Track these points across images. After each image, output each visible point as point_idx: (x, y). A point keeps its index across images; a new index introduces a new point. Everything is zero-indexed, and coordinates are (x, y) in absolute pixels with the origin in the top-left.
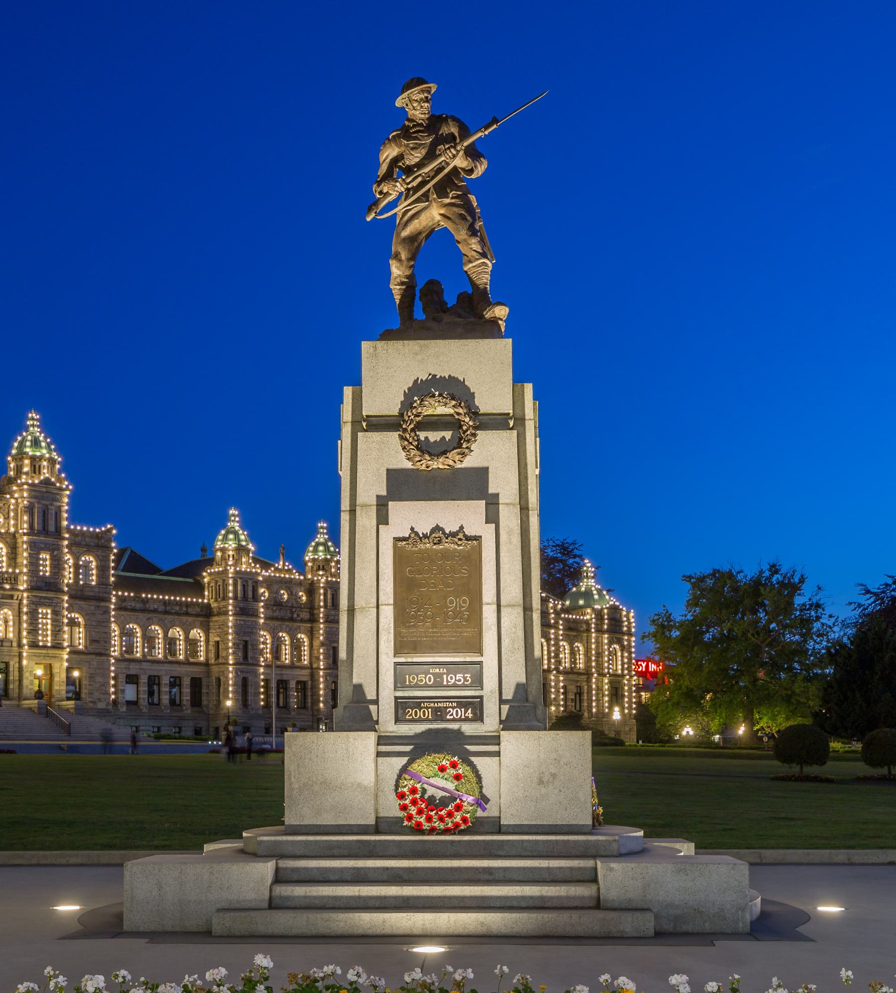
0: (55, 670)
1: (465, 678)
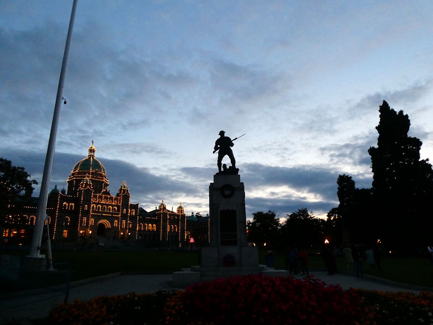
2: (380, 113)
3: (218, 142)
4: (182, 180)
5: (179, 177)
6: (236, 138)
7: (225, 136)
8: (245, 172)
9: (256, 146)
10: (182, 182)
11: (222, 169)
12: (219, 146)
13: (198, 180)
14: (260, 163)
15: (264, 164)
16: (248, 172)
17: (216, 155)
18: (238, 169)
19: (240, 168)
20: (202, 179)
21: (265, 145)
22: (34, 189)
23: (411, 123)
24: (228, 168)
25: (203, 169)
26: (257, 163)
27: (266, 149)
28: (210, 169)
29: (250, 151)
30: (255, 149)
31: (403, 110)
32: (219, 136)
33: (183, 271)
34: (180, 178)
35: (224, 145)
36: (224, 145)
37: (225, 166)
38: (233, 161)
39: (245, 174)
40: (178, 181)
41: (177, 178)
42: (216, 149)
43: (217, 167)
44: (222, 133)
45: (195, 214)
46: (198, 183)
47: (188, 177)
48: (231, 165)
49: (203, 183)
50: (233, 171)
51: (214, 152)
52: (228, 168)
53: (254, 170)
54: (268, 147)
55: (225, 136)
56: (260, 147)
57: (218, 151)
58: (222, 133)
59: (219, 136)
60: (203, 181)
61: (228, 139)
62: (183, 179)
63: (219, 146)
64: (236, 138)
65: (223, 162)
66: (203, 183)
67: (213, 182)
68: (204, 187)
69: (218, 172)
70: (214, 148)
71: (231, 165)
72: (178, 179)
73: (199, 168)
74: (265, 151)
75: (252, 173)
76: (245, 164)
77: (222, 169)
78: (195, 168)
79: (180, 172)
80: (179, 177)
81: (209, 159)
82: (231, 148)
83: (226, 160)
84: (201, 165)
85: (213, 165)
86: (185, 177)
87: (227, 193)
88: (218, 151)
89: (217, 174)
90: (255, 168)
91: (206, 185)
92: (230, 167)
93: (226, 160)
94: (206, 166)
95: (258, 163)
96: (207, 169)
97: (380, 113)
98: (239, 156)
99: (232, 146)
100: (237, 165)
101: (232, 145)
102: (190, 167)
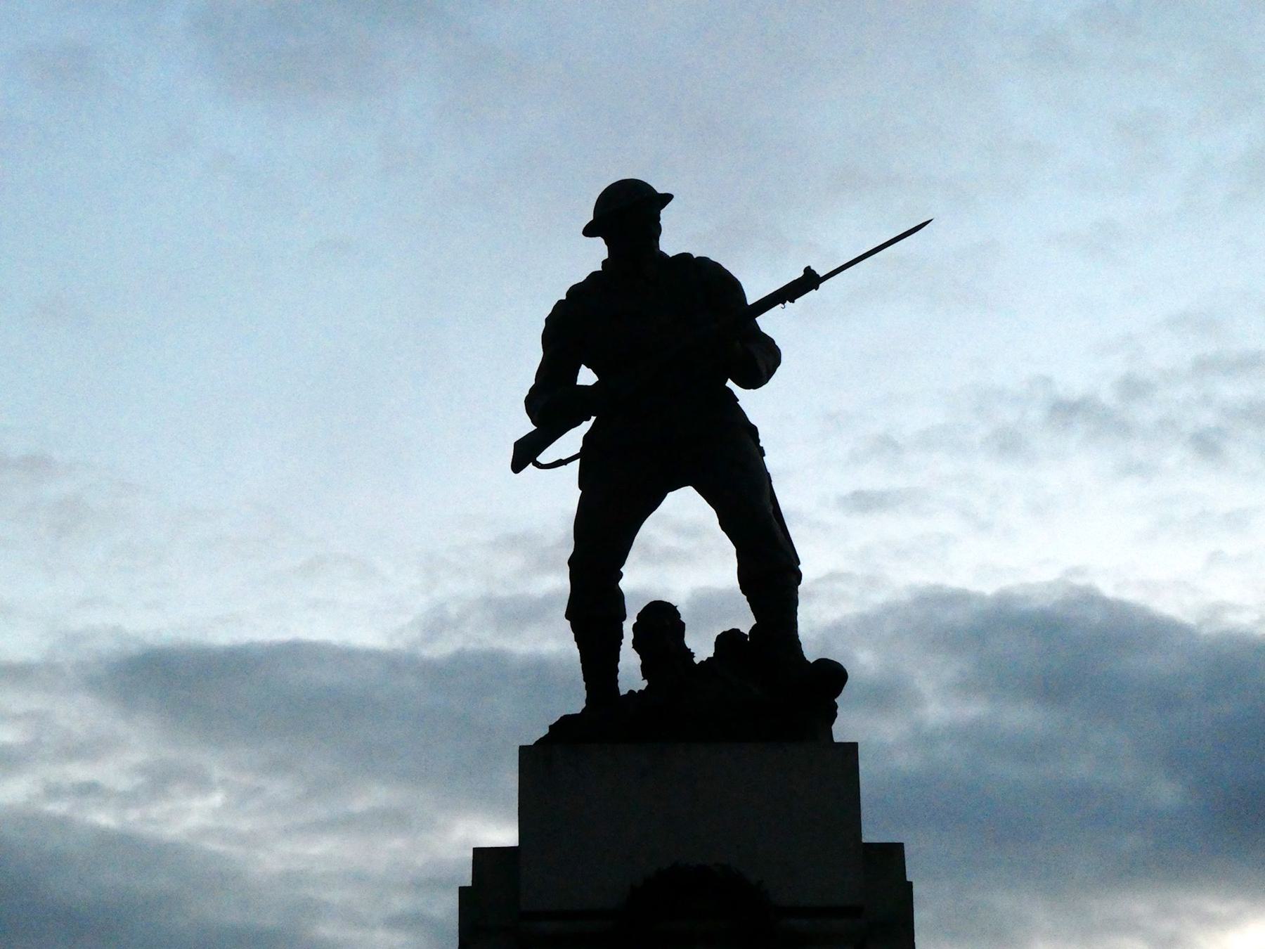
2: (564, 298)
3: (573, 327)
4: (104, 818)
5: (79, 772)
6: (809, 281)
7: (670, 244)
8: (939, 708)
9: (1078, 376)
10: (109, 842)
11: (630, 669)
12: (586, 377)
13: (320, 811)
14: (1131, 596)
15: (1172, 606)
16: (974, 710)
17: (555, 493)
18: (831, 676)
19: (862, 662)
20: (375, 795)
21: (1204, 366)
22: (589, 231)
23: (542, 326)
24: (701, 646)
25: (393, 663)
26: (1090, 598)
27: (1207, 418)
28: (475, 675)
29: (1008, 444)
30: (1066, 411)
32: (595, 253)
34: (89, 790)
35: (653, 368)
36: (653, 368)
37: (662, 621)
39: (925, 739)
40: (62, 823)
41: (54, 792)
42: (550, 405)
43: (558, 644)
44: (627, 213)
46: (322, 850)
47: (200, 782)
48: (745, 622)
49: (389, 850)
50: (774, 685)
51: (525, 453)
52: (701, 646)
53: (1051, 687)
54: (1233, 391)
55: (670, 244)
56: (1133, 388)
57: (571, 441)
58: (627, 213)
59: (595, 253)
60: (395, 820)
61: (708, 283)
62: (128, 799)
63: (586, 377)
64: (809, 281)
65: (640, 580)
66: (389, 850)
67: (505, 835)
68: (400, 903)
69: (576, 702)
70: (533, 404)
71: (745, 622)
72: (58, 808)
73: (346, 656)
74: (1207, 445)
75: (1022, 717)
76: (937, 599)
77: (630, 669)
78: (296, 652)
79: (78, 714)
80: (79, 772)
81: (443, 536)
82: (750, 401)
83: (683, 558)
84: (360, 607)
85: (516, 613)
86: (160, 780)
88: (571, 441)
89: (564, 729)
90: (1066, 656)
91: (426, 884)
92: (728, 640)
94: (437, 624)
95: (1108, 590)
96: (442, 675)
97: (564, 298)
98: (864, 502)
99: (757, 375)
100: (817, 622)
101: (760, 362)
102: (223, 637)
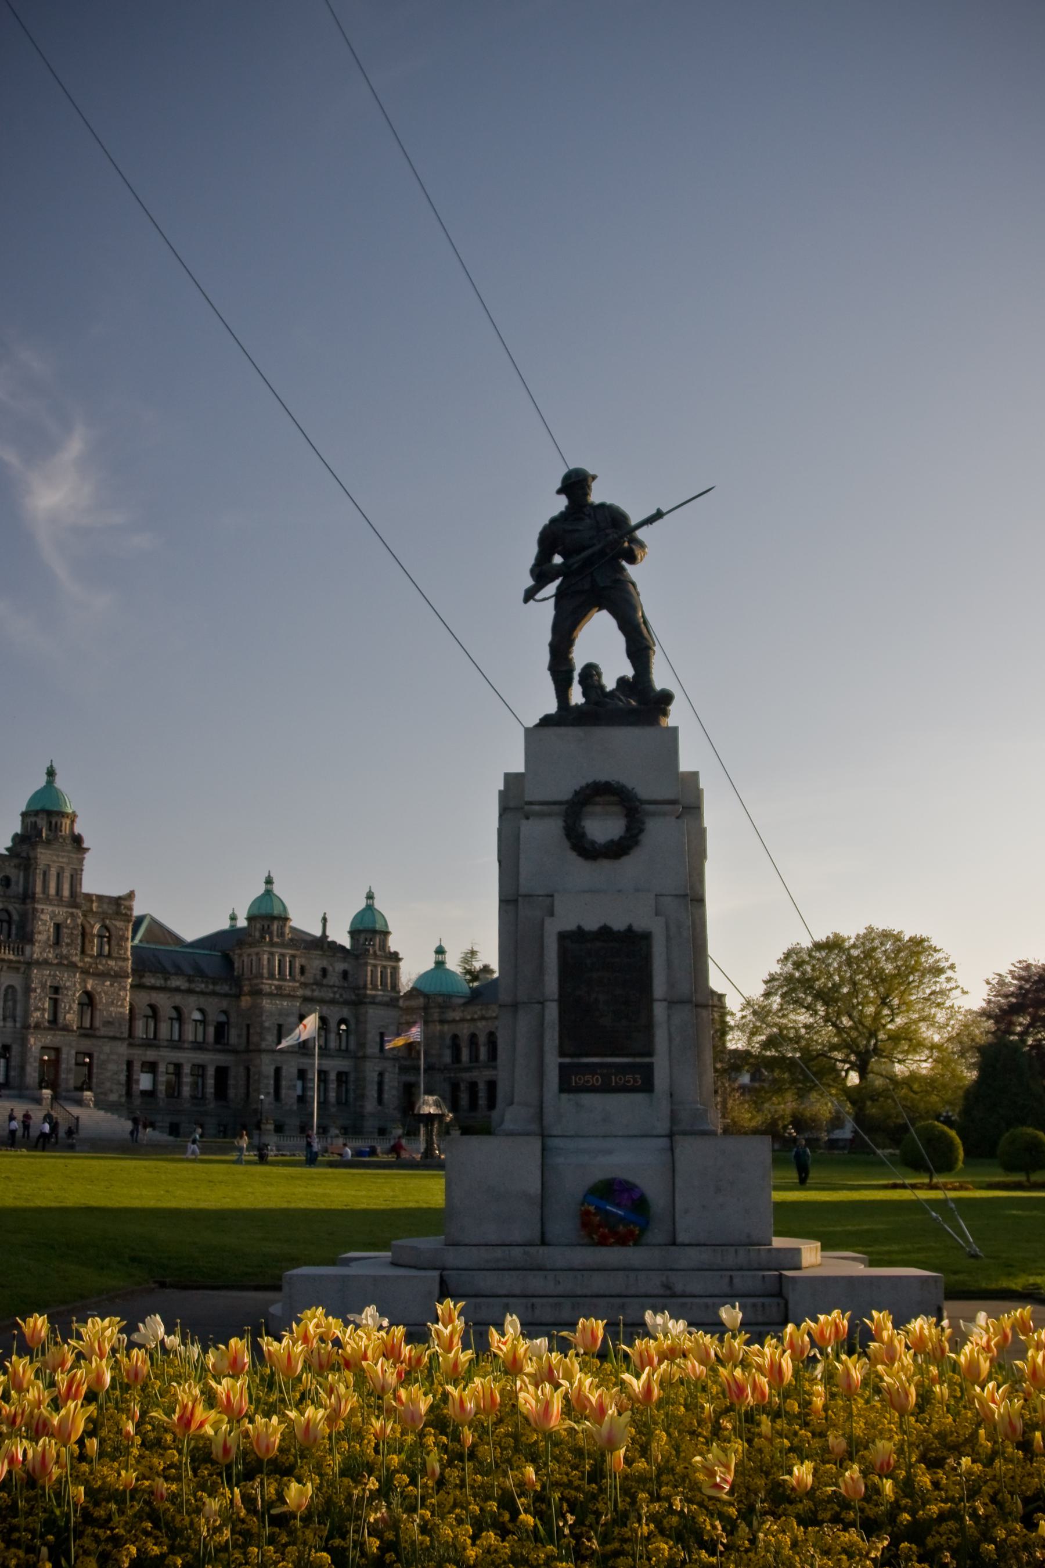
0: (284, 1073)
1: (635, 1081)
3: (550, 539)
6: (659, 515)
17: (544, 612)
31: (78, 813)
32: (562, 503)
33: (347, 1262)
38: (639, 649)
42: (541, 574)
44: (575, 485)
45: (453, 964)
51: (529, 595)
57: (551, 589)
58: (575, 485)
59: (562, 503)
61: (613, 520)
63: (558, 559)
64: (659, 515)
65: (580, 656)
77: (577, 696)
83: (600, 643)
87: (602, 827)
88: (551, 589)
92: (622, 681)
93: (600, 643)
99: (632, 559)
